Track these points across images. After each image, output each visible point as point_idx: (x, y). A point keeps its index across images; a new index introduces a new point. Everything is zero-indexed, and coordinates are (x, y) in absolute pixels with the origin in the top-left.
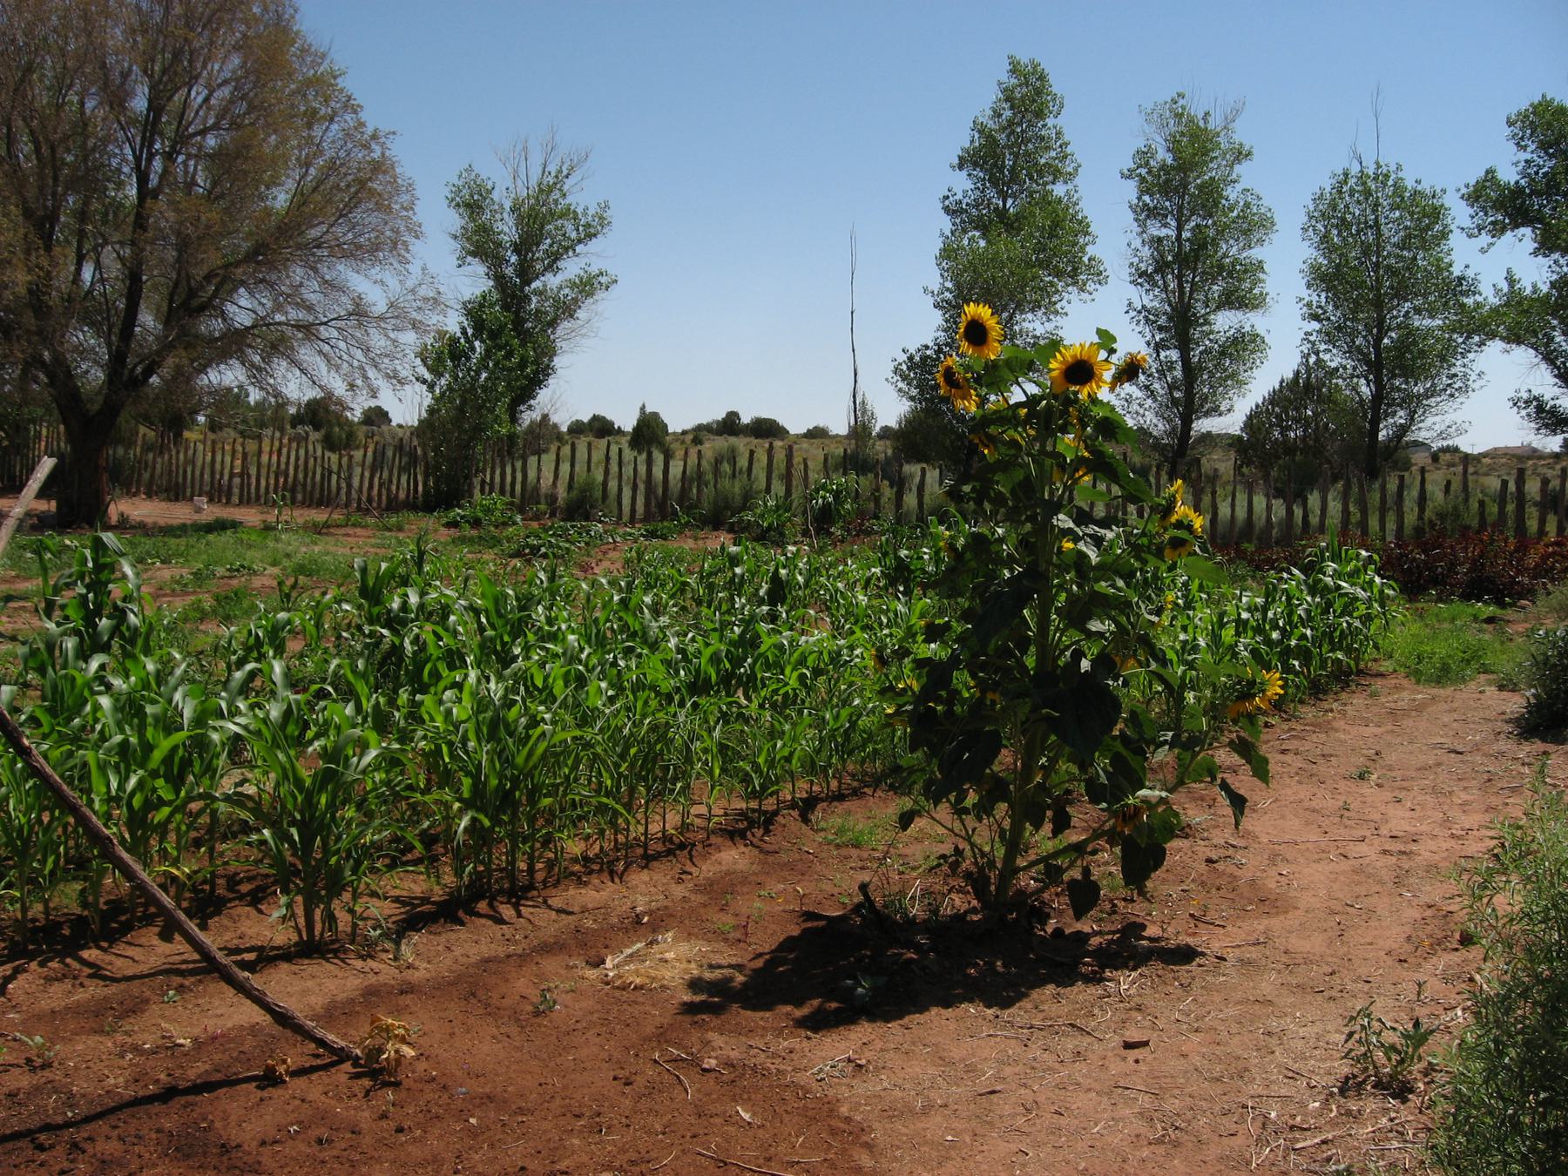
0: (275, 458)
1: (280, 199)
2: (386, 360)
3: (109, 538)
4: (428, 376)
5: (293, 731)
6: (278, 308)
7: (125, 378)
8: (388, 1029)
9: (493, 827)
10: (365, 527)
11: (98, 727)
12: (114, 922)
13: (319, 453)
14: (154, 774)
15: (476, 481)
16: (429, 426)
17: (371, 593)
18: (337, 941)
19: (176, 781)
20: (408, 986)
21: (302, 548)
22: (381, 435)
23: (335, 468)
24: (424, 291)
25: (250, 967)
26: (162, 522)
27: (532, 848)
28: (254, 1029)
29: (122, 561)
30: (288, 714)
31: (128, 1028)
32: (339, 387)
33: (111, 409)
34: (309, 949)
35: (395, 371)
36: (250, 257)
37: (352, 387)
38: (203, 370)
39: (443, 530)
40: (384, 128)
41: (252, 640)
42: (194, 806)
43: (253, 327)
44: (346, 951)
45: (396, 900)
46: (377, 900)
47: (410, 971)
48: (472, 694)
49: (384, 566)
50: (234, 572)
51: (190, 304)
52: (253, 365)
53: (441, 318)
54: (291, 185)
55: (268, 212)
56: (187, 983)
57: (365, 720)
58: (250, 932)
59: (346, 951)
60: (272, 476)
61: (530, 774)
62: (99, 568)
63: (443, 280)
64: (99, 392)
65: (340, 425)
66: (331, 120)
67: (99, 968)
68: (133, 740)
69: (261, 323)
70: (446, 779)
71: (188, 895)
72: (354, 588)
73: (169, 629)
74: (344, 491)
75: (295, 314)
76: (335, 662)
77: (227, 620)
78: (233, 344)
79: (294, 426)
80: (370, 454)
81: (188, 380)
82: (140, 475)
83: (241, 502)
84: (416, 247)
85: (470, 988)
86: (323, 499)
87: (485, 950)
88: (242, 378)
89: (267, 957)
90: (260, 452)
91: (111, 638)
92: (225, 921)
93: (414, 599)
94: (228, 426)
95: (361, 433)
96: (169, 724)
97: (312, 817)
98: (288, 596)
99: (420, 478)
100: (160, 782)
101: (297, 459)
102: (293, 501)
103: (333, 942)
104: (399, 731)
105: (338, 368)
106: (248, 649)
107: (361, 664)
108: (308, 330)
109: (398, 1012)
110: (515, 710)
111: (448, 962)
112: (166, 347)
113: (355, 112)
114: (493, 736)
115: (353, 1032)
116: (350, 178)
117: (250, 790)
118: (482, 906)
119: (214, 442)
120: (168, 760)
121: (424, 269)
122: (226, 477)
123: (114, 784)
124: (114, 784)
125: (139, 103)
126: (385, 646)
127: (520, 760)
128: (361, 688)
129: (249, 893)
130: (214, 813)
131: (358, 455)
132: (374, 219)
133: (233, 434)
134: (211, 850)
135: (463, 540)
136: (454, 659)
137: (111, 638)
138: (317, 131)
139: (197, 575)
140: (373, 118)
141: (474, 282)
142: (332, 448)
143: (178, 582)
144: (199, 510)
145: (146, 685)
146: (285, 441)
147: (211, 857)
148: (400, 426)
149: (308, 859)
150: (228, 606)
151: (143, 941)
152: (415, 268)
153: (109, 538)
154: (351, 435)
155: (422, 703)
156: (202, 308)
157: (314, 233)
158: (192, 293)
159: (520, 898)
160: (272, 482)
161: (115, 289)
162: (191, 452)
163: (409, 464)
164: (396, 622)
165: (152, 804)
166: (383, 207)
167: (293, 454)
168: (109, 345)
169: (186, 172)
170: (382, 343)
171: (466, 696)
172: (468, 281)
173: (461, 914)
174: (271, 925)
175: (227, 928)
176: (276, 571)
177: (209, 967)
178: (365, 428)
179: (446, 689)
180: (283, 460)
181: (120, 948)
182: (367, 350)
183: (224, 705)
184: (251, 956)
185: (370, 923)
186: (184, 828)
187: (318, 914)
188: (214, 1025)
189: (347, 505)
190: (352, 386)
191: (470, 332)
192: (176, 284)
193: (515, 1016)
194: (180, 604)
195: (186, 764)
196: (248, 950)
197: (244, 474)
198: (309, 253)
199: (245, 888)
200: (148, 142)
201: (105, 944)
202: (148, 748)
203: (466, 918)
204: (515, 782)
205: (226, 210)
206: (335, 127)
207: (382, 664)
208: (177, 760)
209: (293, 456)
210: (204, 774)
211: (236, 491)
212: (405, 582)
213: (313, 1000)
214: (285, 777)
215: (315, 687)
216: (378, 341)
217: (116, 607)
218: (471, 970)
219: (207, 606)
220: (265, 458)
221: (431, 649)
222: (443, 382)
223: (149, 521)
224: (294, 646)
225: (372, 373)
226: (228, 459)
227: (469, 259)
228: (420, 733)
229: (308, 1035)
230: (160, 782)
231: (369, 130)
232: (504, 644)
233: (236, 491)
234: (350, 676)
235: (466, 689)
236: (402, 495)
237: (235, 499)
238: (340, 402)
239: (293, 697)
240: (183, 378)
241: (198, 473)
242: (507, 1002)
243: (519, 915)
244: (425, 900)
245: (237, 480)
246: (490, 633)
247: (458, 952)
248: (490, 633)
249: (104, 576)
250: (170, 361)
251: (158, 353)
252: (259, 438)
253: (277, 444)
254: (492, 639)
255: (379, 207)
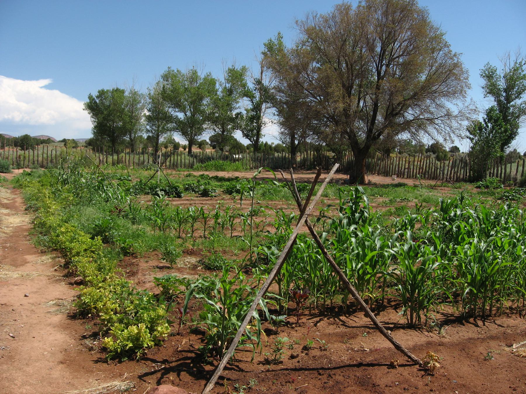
0: (419, 163)
1: (423, 77)
2: (457, 131)
3: (360, 188)
4: (472, 136)
5: (413, 254)
6: (422, 113)
7: (372, 137)
8: (432, 356)
9: (477, 293)
10: (448, 187)
11: (351, 248)
12: (352, 309)
13: (434, 162)
14: (366, 264)
15: (488, 172)
16: (470, 154)
17: (445, 210)
18: (421, 325)
19: (373, 267)
20: (444, 344)
21: (425, 193)
22: (456, 155)
23: (439, 167)
24: (472, 107)
25: (391, 329)
26: (381, 183)
27: (491, 302)
28: (389, 349)
29: (364, 195)
30: (410, 248)
31: (351, 342)
32: (441, 140)
33: (367, 147)
34: (411, 326)
35: (460, 134)
36: (413, 97)
37: (445, 140)
38: (397, 134)
39: (475, 189)
40: (458, 52)
41: (404, 223)
42: (378, 275)
43: (413, 120)
44: (423, 329)
45: (442, 314)
46: (434, 314)
47: (443, 339)
48: (475, 246)
49: (449, 201)
50: (403, 200)
51: (392, 113)
52: (413, 133)
53: (477, 116)
54: (426, 72)
55: (419, 82)
56: (370, 331)
57: (438, 252)
58: (393, 318)
59: (423, 329)
60: (418, 169)
61: (492, 276)
62: (357, 197)
63: (478, 102)
64: (363, 141)
65: (442, 152)
66: (440, 50)
67: (345, 323)
68: (361, 253)
69: (416, 119)
70: (464, 275)
71: (375, 303)
72: (439, 208)
73: (378, 218)
74: (441, 174)
75: (427, 115)
76: (429, 233)
77: (399, 216)
78: (407, 125)
79: (427, 153)
80: (451, 162)
81: (392, 137)
82: (376, 168)
83: (407, 177)
84: (469, 92)
85: (463, 347)
86: (434, 177)
87: (471, 335)
88: (409, 137)
89: (397, 327)
90: (414, 161)
91: (359, 220)
92: (385, 313)
93: (459, 213)
94: (405, 152)
95: (449, 155)
96: (373, 249)
97: (415, 283)
98: (419, 209)
99: (468, 171)
100: (368, 267)
101: (426, 163)
102: (425, 177)
103: (419, 325)
104: (448, 257)
105: (441, 133)
106: (402, 226)
107: (438, 234)
108: (431, 121)
109: (436, 351)
110: (489, 253)
111: (457, 337)
112: (385, 127)
113: (448, 47)
114: (480, 262)
115: (421, 356)
116: (446, 69)
117: (397, 272)
118: (472, 320)
119: (399, 157)
120: (371, 260)
121: (471, 99)
122: (403, 169)
123: (354, 266)
124: (354, 266)
125: (378, 49)
126: (448, 229)
127: (489, 271)
128: (437, 242)
129: (394, 305)
130: (385, 278)
131: (447, 162)
132: (454, 83)
133: (407, 155)
134: (383, 290)
135: (481, 193)
136: (470, 234)
137: (359, 220)
138: (435, 55)
139: (391, 201)
140: (454, 49)
141: (490, 102)
142: (439, 160)
143: (384, 203)
144: (393, 180)
145: (367, 235)
146: (423, 157)
147: (383, 291)
148: (463, 153)
149: (413, 296)
150: (399, 212)
151: (359, 316)
152: (468, 99)
153: (360, 188)
154: (445, 156)
155: (457, 248)
156: (397, 114)
157: (434, 88)
158: (393, 110)
159: (485, 319)
160: (418, 171)
161: (370, 109)
162: (392, 161)
163: (464, 166)
164: (451, 220)
165: (365, 273)
166: (458, 79)
167: (425, 162)
168: (367, 126)
169: (393, 70)
170: (456, 125)
171: (472, 247)
172: (487, 103)
173: (464, 321)
174: (399, 316)
175: (386, 316)
176: (416, 200)
177: (376, 327)
178: (451, 153)
179: (466, 244)
180: (422, 163)
181: (352, 317)
182: (451, 127)
183: (390, 244)
184: (392, 326)
185: (432, 320)
186: (375, 282)
187: (415, 315)
188: (377, 346)
189: (442, 180)
190: (445, 140)
191: (487, 121)
192: (389, 107)
193: (477, 359)
194: (384, 210)
195: (377, 262)
196: (391, 324)
197: (409, 168)
198: (433, 95)
199: (393, 303)
200: (381, 61)
201: (347, 315)
202: (365, 255)
203: (465, 323)
204: (487, 278)
205: (405, 83)
206: (441, 52)
207: (446, 234)
208: (374, 260)
209: (425, 163)
210: (382, 265)
211: (406, 174)
212: (456, 207)
213: (410, 343)
214: (407, 268)
215: (421, 240)
216: (454, 124)
217: (361, 210)
218: (464, 341)
219: (392, 211)
220: (416, 163)
221: (462, 230)
222: (477, 138)
223: (378, 183)
224: (417, 226)
225: (452, 135)
226: (404, 163)
227: (488, 95)
228: (455, 258)
229: (406, 354)
230: (368, 267)
231: (453, 53)
232: (488, 230)
233: (406, 174)
234: (434, 237)
235: (473, 244)
236: (461, 177)
237: (406, 176)
238: (441, 145)
239: (412, 243)
240: (390, 137)
241: (394, 167)
242: (475, 354)
243: (484, 325)
244: (452, 315)
245: (406, 170)
246: (483, 226)
247: (461, 334)
248: (483, 226)
249: (358, 200)
250: (386, 131)
251: (382, 128)
252: (414, 156)
253: (420, 158)
254: (484, 228)
255: (456, 79)
